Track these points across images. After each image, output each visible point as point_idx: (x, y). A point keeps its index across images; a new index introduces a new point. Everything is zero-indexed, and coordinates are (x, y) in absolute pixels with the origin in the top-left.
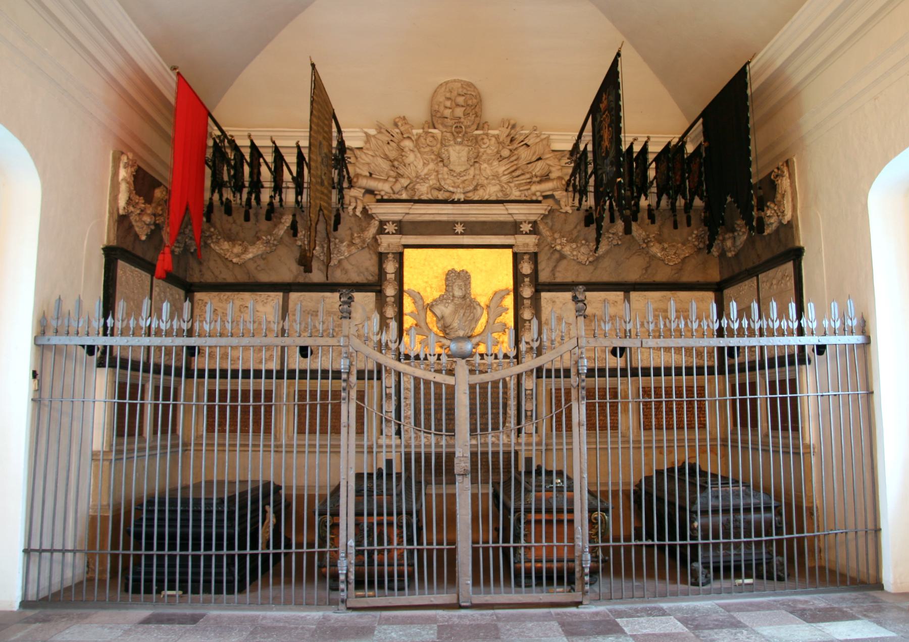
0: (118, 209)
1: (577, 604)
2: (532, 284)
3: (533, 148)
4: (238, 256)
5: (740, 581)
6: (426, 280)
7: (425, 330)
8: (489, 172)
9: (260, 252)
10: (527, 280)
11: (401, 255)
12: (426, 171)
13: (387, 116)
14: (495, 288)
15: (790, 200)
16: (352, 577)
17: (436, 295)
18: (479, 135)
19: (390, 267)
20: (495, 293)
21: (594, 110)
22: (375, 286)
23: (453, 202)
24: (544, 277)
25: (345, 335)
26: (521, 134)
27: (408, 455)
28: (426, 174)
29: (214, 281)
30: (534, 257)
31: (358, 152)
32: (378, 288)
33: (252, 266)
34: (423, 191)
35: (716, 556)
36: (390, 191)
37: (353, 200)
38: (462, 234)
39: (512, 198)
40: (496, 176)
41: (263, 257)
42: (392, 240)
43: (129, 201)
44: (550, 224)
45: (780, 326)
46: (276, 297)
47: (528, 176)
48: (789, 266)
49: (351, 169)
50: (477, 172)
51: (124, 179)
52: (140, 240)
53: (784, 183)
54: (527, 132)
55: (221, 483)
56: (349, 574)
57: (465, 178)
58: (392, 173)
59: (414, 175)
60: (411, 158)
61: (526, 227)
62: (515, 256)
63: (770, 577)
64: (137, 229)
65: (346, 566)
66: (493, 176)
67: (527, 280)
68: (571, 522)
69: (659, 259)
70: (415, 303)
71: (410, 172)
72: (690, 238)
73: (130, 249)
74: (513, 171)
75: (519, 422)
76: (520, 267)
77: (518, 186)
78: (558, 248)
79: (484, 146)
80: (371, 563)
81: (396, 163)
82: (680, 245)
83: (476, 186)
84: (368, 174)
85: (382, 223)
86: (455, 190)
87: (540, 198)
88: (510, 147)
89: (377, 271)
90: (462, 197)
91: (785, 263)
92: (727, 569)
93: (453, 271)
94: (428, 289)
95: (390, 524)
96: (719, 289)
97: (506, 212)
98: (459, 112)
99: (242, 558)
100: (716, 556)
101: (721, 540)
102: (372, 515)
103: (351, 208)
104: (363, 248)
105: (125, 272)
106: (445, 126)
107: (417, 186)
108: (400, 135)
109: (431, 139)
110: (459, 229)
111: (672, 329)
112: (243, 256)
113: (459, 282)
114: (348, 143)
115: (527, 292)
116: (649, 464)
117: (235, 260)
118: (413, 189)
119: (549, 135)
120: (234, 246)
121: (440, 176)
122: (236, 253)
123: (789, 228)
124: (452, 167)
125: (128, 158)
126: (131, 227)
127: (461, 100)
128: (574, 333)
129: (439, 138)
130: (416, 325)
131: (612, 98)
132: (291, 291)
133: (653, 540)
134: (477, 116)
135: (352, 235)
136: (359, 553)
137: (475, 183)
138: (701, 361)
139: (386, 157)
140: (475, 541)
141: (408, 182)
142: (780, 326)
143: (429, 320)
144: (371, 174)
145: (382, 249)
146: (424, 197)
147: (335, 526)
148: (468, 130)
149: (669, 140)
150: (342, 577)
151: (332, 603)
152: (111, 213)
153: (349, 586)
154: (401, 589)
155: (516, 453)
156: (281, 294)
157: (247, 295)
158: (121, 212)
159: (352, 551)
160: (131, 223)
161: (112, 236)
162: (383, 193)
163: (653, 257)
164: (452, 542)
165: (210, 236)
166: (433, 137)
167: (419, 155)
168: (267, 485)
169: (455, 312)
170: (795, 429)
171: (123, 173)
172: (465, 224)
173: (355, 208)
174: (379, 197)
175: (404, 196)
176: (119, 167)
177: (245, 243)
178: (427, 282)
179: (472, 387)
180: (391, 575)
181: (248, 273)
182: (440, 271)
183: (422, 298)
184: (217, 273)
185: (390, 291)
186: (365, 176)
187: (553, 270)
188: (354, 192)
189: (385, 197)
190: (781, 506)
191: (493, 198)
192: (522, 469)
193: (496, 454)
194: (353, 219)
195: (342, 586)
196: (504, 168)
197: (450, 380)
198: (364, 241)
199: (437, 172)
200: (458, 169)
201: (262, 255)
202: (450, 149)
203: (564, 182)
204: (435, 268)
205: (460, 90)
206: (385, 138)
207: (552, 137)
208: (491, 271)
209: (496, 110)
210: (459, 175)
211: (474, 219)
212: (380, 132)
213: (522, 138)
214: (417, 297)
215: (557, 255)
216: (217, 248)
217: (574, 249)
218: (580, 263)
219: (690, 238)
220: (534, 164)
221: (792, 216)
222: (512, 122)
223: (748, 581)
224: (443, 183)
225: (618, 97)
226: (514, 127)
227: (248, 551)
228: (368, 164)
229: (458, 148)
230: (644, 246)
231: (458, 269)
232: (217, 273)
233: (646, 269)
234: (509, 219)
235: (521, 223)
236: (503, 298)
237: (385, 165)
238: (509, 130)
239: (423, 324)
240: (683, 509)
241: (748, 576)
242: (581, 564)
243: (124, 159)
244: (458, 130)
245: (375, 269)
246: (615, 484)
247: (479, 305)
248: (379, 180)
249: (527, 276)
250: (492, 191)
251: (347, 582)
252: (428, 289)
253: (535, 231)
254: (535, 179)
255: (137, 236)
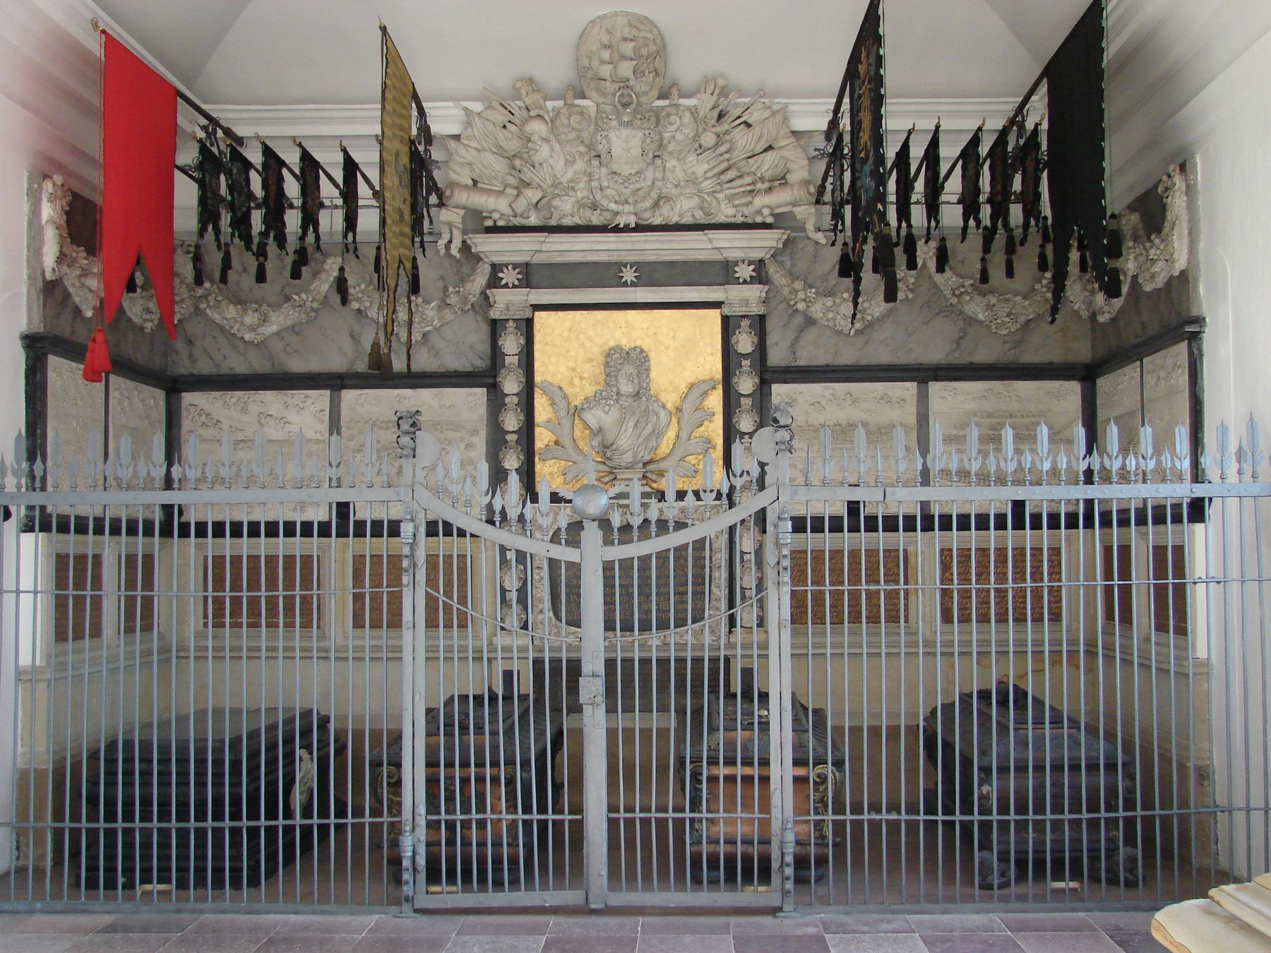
0: (43, 272)
1: (774, 911)
2: (757, 373)
3: (757, 129)
4: (253, 329)
5: (1061, 885)
6: (571, 364)
7: (572, 452)
8: (680, 175)
9: (289, 323)
10: (746, 363)
11: (529, 322)
12: (570, 174)
13: (502, 78)
14: (691, 379)
15: (1186, 232)
16: (422, 861)
17: (590, 390)
18: (663, 108)
19: (511, 344)
20: (691, 387)
21: (851, 74)
22: (485, 376)
23: (617, 229)
24: (777, 356)
25: (435, 460)
26: (737, 105)
27: (538, 663)
28: (569, 181)
29: (214, 371)
30: (760, 324)
31: (453, 144)
32: (491, 381)
33: (276, 347)
34: (566, 210)
35: (1022, 842)
36: (508, 211)
37: (445, 229)
38: (633, 284)
39: (721, 219)
40: (692, 181)
41: (294, 329)
42: (512, 298)
43: (62, 258)
44: (788, 264)
45: (1123, 467)
46: (320, 399)
47: (748, 180)
48: (1181, 350)
49: (436, 174)
50: (659, 175)
51: (51, 221)
52: (83, 318)
53: (1177, 204)
54: (747, 100)
55: (219, 712)
56: (417, 857)
57: (638, 186)
58: (511, 180)
59: (549, 182)
60: (543, 152)
61: (745, 272)
62: (725, 320)
63: (1113, 881)
64: (77, 300)
65: (413, 843)
66: (688, 182)
67: (746, 363)
68: (765, 780)
69: (981, 323)
70: (553, 404)
71: (541, 177)
72: (1037, 286)
73: (67, 334)
74: (723, 172)
75: (731, 604)
76: (733, 340)
77: (729, 199)
78: (801, 306)
79: (672, 128)
80: (451, 842)
81: (517, 163)
82: (1019, 298)
83: (660, 198)
84: (470, 182)
85: (496, 268)
86: (620, 208)
87: (770, 220)
88: (717, 130)
89: (488, 351)
90: (632, 221)
91: (1177, 343)
92: (1040, 864)
93: (616, 349)
94: (577, 381)
95: (496, 780)
96: (1086, 376)
97: (709, 246)
98: (626, 69)
99: (254, 832)
100: (1022, 842)
101: (1031, 816)
102: (453, 765)
103: (442, 242)
104: (464, 312)
105: (60, 375)
106: (602, 94)
107: (556, 202)
108: (524, 112)
109: (578, 118)
110: (629, 275)
111: (996, 449)
112: (262, 330)
113: (629, 369)
114: (435, 128)
115: (746, 384)
116: (948, 682)
117: (247, 337)
118: (549, 205)
119: (787, 105)
120: (245, 312)
121: (594, 184)
122: (255, 323)
123: (1183, 282)
124: (615, 167)
125: (54, 185)
126: (67, 296)
127: (628, 48)
128: (851, 448)
129: (593, 113)
130: (557, 443)
131: (872, 60)
132: (344, 387)
133: (899, 813)
134: (657, 74)
135: (446, 289)
136: (433, 826)
137: (654, 195)
138: (567, 636)
139: (501, 152)
140: (613, 808)
141: (539, 195)
142: (1123, 467)
143: (577, 433)
144: (475, 182)
145: (495, 314)
146: (567, 221)
147: (396, 785)
148: (643, 100)
149: (973, 125)
150: (406, 863)
151: (396, 901)
152: (32, 278)
153: (418, 877)
154: (514, 882)
155: (727, 660)
156: (328, 392)
157: (269, 396)
158: (49, 276)
159: (422, 822)
160: (66, 290)
161: (37, 318)
162: (496, 216)
163: (971, 321)
164: (577, 808)
165: (205, 297)
166: (582, 114)
167: (557, 147)
168: (306, 714)
169: (622, 420)
170: (1182, 630)
171: (48, 211)
172: (638, 266)
173: (450, 242)
174: (489, 223)
175: (533, 220)
176: (41, 199)
177: (265, 307)
178: (573, 369)
179: (608, 567)
180: (498, 861)
181: (271, 357)
182: (596, 350)
183: (566, 397)
184: (218, 357)
185: (511, 385)
186: (466, 186)
187: (792, 345)
188: (445, 215)
189: (501, 223)
190: (1134, 762)
191: (687, 220)
192: (737, 688)
193: (698, 661)
194: (447, 262)
195: (406, 876)
196: (706, 167)
197: (564, 554)
198: (465, 300)
199: (590, 174)
200: (626, 170)
201: (293, 327)
202: (612, 136)
203: (812, 190)
204: (588, 345)
205: (626, 30)
206: (500, 117)
207: (791, 108)
208: (684, 349)
209: (687, 65)
210: (627, 180)
211: (653, 258)
212: (489, 107)
213: (737, 112)
214: (557, 395)
215: (799, 320)
216: (216, 316)
217: (828, 309)
218: (840, 333)
219: (1037, 286)
220: (760, 158)
221: (1189, 262)
222: (721, 82)
223: (1073, 884)
224: (599, 196)
225: (880, 60)
226: (724, 93)
227: (174, 823)
228: (470, 164)
229: (625, 132)
230: (954, 300)
231: (626, 343)
232: (218, 358)
233: (958, 342)
234: (718, 257)
235: (736, 263)
236: (705, 394)
237: (499, 166)
238: (714, 98)
239: (567, 442)
240: (967, 762)
241: (1058, 875)
242: (782, 848)
243: (48, 186)
244: (627, 105)
245: (485, 348)
246: (894, 715)
247: (664, 406)
248: (489, 192)
249: (746, 356)
250: (684, 208)
251: (415, 869)
252: (577, 381)
253: (760, 276)
254: (759, 186)
255: (77, 311)
